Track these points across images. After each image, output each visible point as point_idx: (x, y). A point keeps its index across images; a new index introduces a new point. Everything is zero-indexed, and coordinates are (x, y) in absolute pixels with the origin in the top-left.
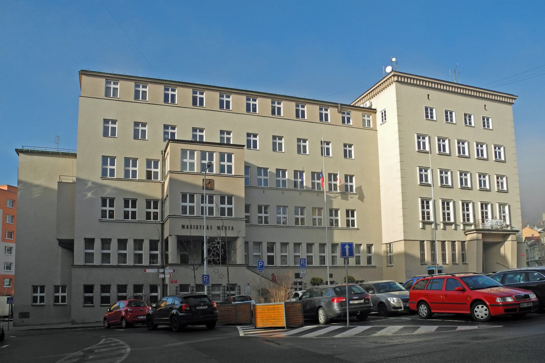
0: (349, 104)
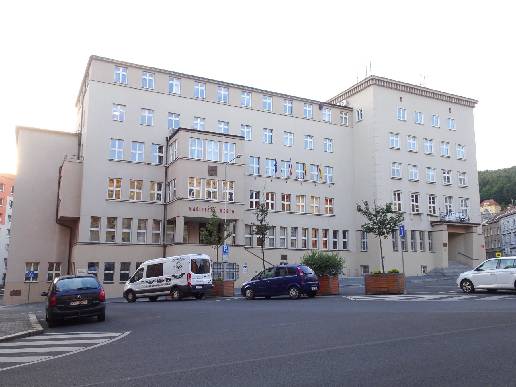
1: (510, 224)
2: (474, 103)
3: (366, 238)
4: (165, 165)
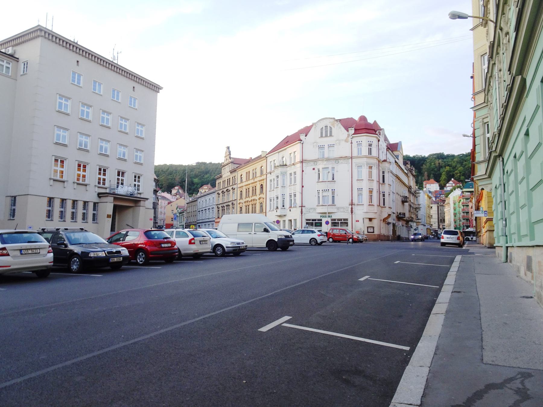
2: (159, 88)
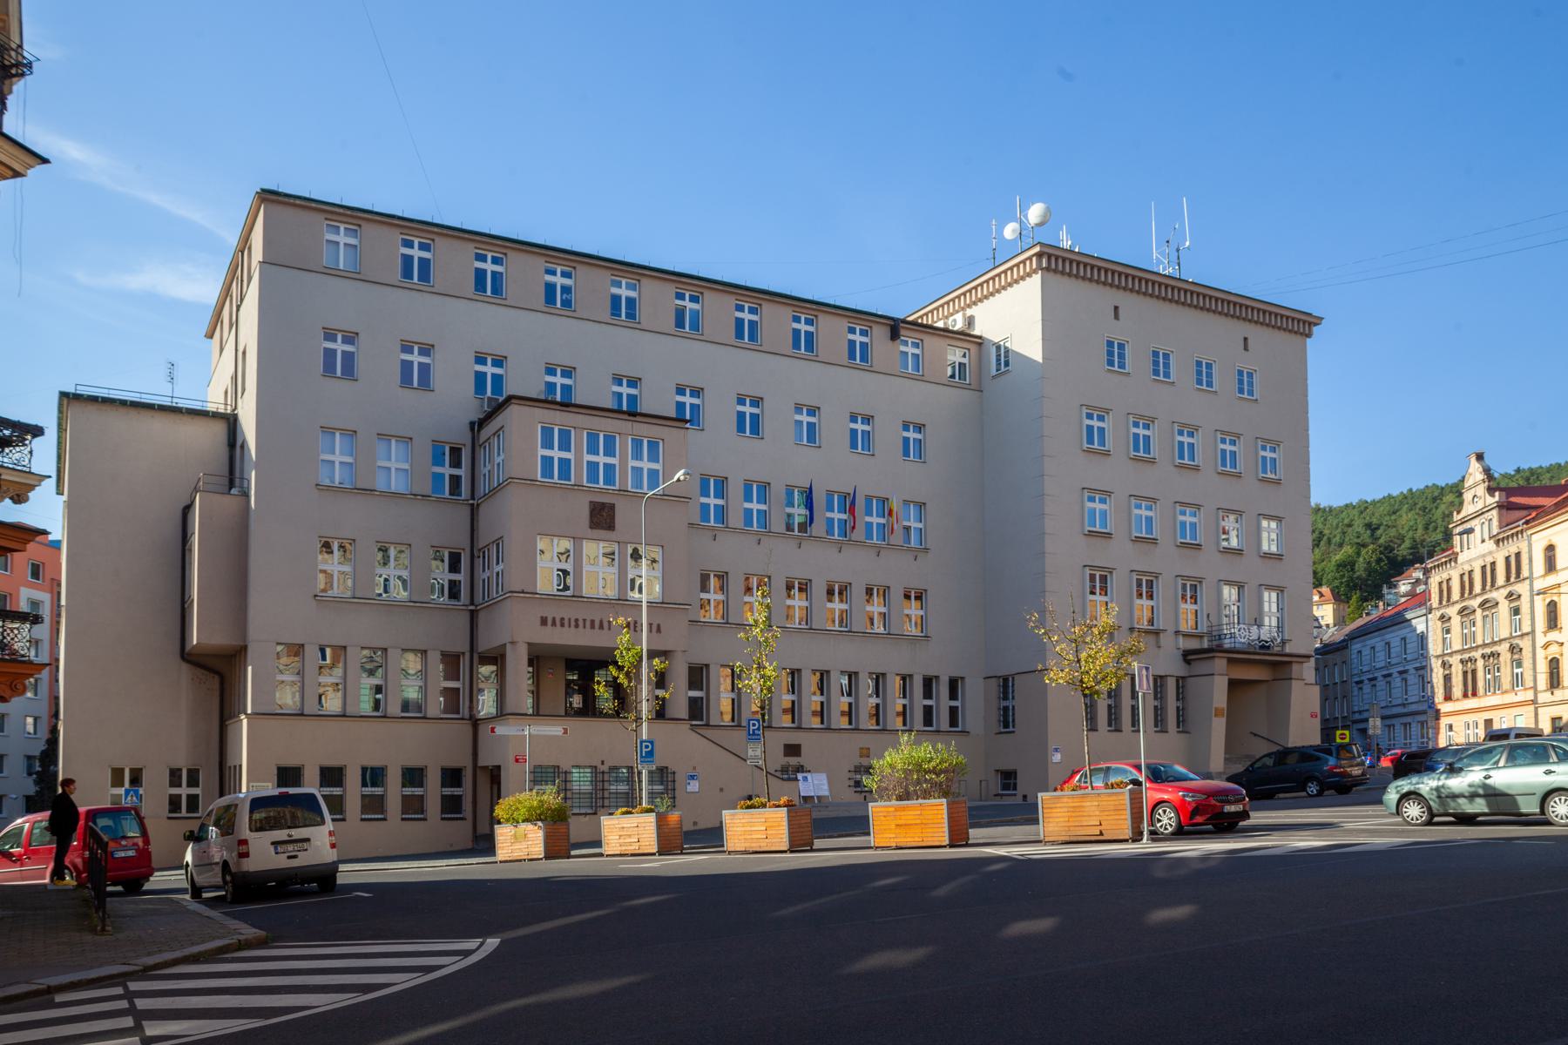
0: (902, 318)
1: (1377, 655)
2: (1310, 324)
3: (1011, 697)
4: (468, 500)
